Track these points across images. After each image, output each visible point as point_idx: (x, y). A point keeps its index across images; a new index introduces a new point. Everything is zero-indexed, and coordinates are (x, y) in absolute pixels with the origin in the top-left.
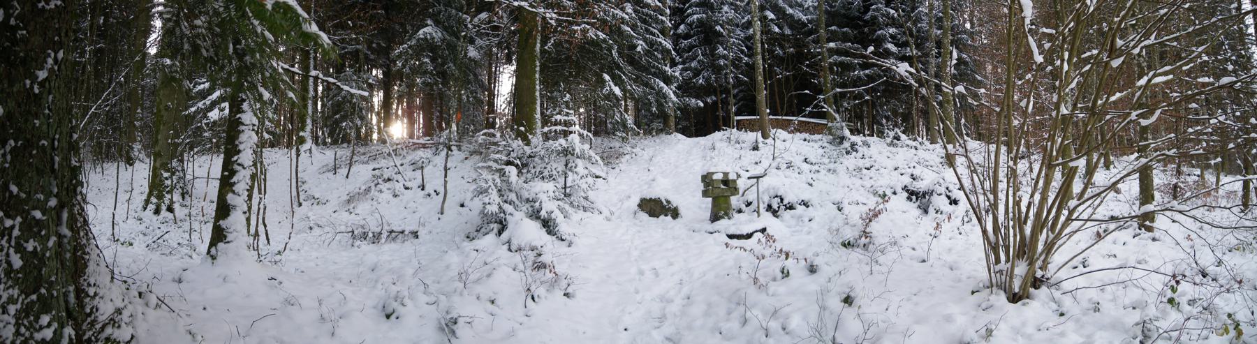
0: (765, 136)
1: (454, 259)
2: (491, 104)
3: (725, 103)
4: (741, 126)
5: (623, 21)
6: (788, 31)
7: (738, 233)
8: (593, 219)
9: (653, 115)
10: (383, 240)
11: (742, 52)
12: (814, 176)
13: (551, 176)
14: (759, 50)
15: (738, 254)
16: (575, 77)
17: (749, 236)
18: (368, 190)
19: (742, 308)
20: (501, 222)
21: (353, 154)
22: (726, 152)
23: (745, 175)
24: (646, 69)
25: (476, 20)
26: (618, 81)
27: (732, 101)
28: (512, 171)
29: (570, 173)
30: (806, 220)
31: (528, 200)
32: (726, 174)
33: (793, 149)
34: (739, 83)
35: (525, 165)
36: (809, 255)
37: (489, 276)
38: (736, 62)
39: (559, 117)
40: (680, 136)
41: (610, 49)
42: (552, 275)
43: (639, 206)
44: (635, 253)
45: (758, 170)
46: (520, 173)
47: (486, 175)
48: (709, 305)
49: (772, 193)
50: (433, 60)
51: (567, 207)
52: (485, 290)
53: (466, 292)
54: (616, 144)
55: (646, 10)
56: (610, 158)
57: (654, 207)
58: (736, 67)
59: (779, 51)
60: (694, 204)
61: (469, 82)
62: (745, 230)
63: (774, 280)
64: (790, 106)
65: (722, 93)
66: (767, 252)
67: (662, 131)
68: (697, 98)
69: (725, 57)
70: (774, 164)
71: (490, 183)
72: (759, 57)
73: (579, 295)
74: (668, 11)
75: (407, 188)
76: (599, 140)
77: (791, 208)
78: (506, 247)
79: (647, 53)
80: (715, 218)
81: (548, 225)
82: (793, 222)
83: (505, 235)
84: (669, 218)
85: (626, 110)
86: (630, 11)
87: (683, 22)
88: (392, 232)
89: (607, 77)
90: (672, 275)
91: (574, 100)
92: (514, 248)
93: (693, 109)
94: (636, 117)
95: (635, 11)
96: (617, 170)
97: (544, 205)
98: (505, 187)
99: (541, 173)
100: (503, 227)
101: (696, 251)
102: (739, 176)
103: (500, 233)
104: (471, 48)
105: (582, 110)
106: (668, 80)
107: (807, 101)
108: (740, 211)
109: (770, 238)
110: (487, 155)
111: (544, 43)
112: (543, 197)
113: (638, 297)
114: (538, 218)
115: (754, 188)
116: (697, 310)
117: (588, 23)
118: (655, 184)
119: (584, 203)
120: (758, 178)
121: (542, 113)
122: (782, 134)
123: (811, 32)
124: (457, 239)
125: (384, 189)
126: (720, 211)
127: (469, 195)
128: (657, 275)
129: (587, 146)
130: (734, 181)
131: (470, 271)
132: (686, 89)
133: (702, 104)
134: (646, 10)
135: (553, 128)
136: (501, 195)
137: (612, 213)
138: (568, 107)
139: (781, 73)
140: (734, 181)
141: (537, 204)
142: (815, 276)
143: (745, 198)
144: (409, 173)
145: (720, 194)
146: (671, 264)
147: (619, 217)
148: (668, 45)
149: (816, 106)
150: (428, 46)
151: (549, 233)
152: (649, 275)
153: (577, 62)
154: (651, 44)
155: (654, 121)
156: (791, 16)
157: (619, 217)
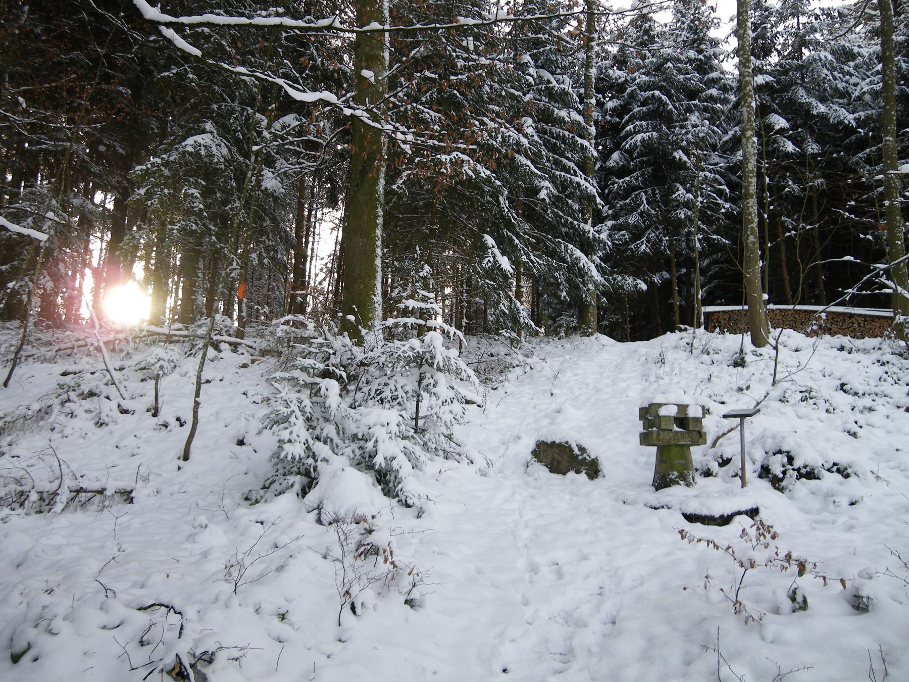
0: (758, 341)
1: (216, 538)
2: (300, 271)
3: (686, 283)
4: (712, 323)
5: (518, 148)
6: (813, 148)
7: (704, 512)
8: (460, 473)
9: (561, 303)
10: (59, 507)
11: (720, 193)
12: (862, 419)
13: (394, 398)
14: (753, 189)
15: (699, 551)
16: (440, 238)
17: (725, 520)
18: (47, 411)
19: (712, 657)
20: (307, 474)
21: (24, 341)
22: (685, 368)
23: (718, 410)
24: (552, 228)
25: (277, 125)
26: (506, 247)
27: (698, 279)
28: (332, 387)
29: (425, 395)
30: (845, 502)
31: (355, 438)
32: (682, 408)
33: (816, 365)
34: (711, 247)
35: (352, 378)
36: (851, 574)
37: (280, 569)
38: (707, 214)
39: (411, 304)
40: (605, 339)
41: (495, 194)
42: (388, 566)
43: (535, 453)
44: (525, 534)
45: (743, 403)
46: (344, 390)
47: (287, 392)
48: (651, 641)
49: (771, 445)
50: (206, 193)
51: (418, 450)
52: (269, 597)
53: (236, 600)
54: (501, 349)
55: (556, 130)
56: (489, 372)
57: (559, 457)
58: (706, 220)
59: (792, 187)
60: (627, 458)
61: (263, 232)
62: (718, 509)
63: (776, 611)
64: (812, 285)
65: (679, 266)
66: (760, 556)
67: (575, 329)
68: (636, 275)
69: (688, 205)
70: (776, 393)
71: (294, 407)
72: (752, 203)
73: (431, 603)
74: (593, 130)
75: (124, 412)
76: (474, 341)
77: (811, 475)
78: (313, 515)
79: (556, 201)
80: (662, 482)
81: (385, 479)
82: (815, 504)
83: (313, 496)
84: (583, 476)
85: (519, 295)
86: (530, 131)
87: (617, 146)
88: (80, 491)
89: (489, 240)
90: (587, 577)
91: (435, 275)
92: (325, 518)
93: (629, 295)
94: (535, 305)
95: (541, 132)
96: (501, 391)
97: (381, 447)
98: (318, 414)
99: (379, 392)
100: (310, 481)
101: (627, 536)
102: (706, 411)
103: (304, 492)
104: (267, 173)
105: (448, 291)
106: (587, 247)
107: (850, 275)
108: (708, 473)
109: (765, 530)
110: (291, 358)
111: (391, 178)
112: (380, 433)
113: (528, 612)
114: (370, 467)
115: (736, 434)
116: (629, 646)
117: (464, 152)
118: (560, 418)
119: (445, 444)
120: (742, 416)
121: (385, 294)
122: (792, 337)
123: (863, 144)
124: (227, 502)
125: (79, 411)
126: (671, 470)
127: (256, 425)
128: (560, 575)
129: (454, 352)
130: (698, 421)
131: (247, 561)
132: (618, 260)
133: (643, 286)
134: (556, 130)
135: (402, 320)
136: (311, 427)
137: (489, 463)
138: (426, 287)
139: (793, 227)
140: (698, 421)
141: (370, 445)
142: (863, 619)
143: (718, 450)
144: (134, 386)
145: (672, 441)
146: (585, 558)
147: (501, 471)
148: (590, 187)
149: (869, 284)
150: (200, 168)
151: (387, 492)
152: (546, 572)
153: (443, 214)
154: (563, 186)
155: (562, 312)
156: (823, 117)
157: (501, 471)
